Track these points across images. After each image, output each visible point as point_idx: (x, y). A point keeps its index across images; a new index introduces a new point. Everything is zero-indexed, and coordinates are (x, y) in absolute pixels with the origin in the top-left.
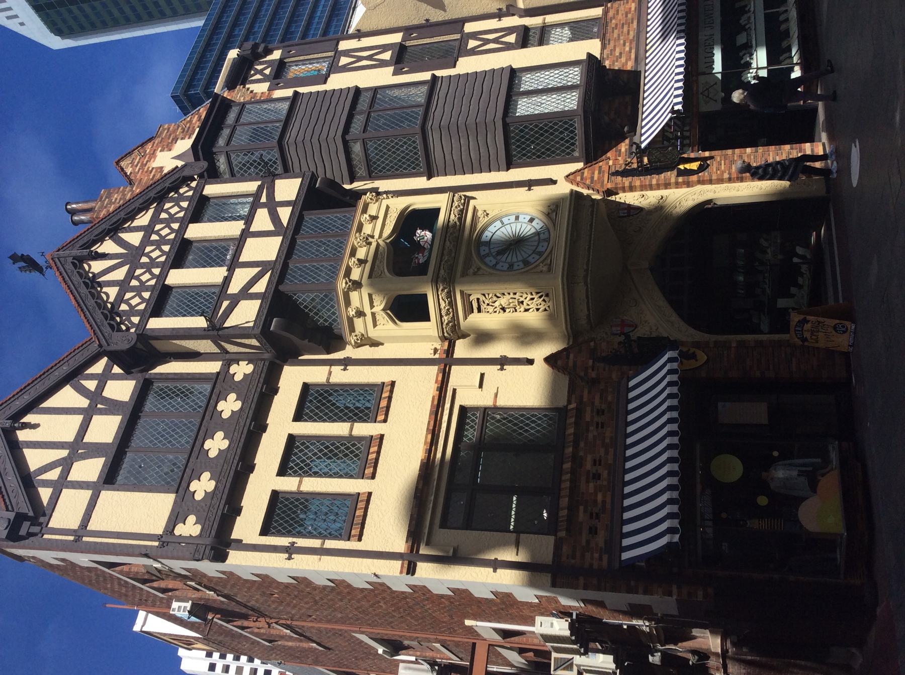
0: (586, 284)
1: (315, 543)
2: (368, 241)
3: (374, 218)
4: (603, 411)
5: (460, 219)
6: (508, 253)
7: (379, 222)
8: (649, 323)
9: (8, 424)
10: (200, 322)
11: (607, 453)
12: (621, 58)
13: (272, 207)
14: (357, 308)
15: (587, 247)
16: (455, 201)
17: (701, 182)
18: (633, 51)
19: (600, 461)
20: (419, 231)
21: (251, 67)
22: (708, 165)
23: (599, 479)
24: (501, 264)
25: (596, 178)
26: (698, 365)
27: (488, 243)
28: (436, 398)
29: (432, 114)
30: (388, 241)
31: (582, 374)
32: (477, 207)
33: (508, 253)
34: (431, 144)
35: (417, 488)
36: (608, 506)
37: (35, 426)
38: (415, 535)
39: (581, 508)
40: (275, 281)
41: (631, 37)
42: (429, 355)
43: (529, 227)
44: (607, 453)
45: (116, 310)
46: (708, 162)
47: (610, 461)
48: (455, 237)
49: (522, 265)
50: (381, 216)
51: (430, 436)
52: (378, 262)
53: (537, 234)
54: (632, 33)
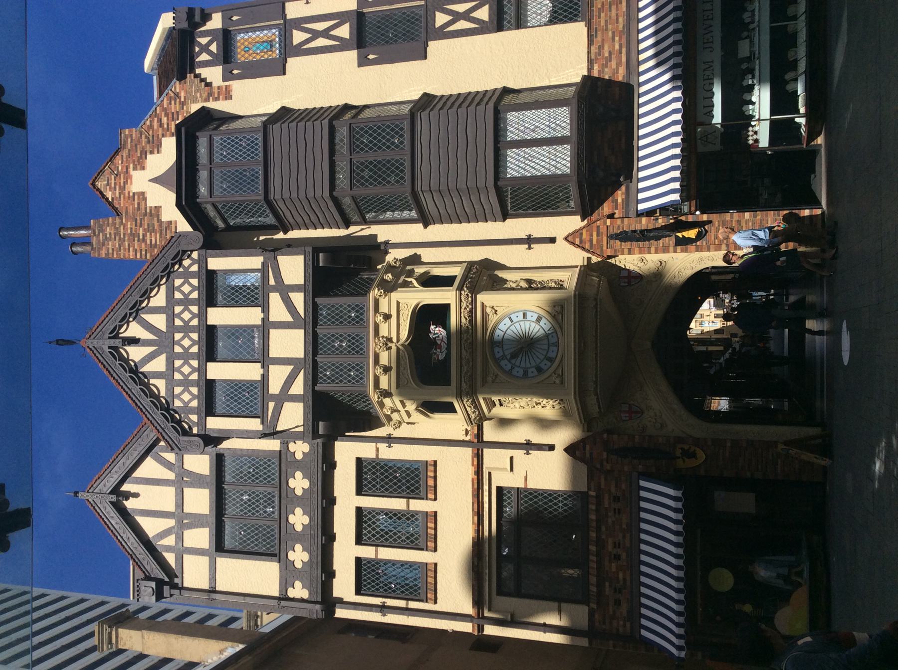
0: (596, 394)
1: (401, 603)
2: (388, 346)
3: (387, 317)
4: (619, 498)
5: (471, 321)
6: (521, 355)
7: (394, 319)
8: (653, 410)
9: (114, 498)
10: (255, 424)
11: (624, 537)
12: (610, 61)
13: (285, 291)
14: (391, 407)
15: (594, 355)
16: (463, 301)
17: (698, 249)
18: (624, 50)
19: (619, 544)
20: (432, 327)
21: (193, 42)
22: (706, 231)
23: (620, 560)
24: (516, 369)
25: (595, 242)
26: (698, 464)
27: (502, 343)
28: (476, 482)
29: (419, 170)
30: (406, 343)
31: (598, 466)
32: (485, 303)
33: (521, 355)
34: (424, 202)
35: (473, 563)
36: (628, 583)
37: (136, 495)
38: (478, 602)
39: (607, 584)
40: (310, 383)
41: (621, 27)
42: (461, 437)
43: (538, 327)
44: (624, 537)
45: (140, 312)
46: (706, 227)
47: (628, 545)
48: (470, 343)
49: (536, 373)
50: (394, 313)
51: (476, 518)
52: (402, 369)
53: (547, 336)
54: (621, 20)
